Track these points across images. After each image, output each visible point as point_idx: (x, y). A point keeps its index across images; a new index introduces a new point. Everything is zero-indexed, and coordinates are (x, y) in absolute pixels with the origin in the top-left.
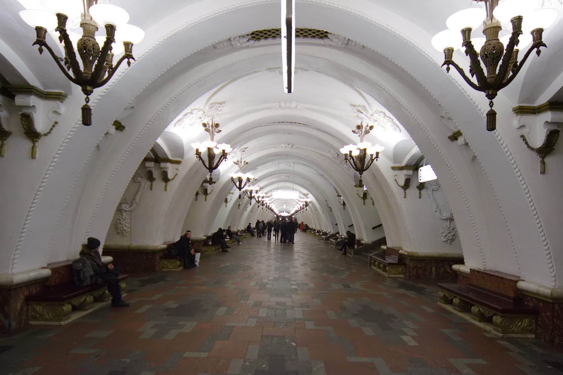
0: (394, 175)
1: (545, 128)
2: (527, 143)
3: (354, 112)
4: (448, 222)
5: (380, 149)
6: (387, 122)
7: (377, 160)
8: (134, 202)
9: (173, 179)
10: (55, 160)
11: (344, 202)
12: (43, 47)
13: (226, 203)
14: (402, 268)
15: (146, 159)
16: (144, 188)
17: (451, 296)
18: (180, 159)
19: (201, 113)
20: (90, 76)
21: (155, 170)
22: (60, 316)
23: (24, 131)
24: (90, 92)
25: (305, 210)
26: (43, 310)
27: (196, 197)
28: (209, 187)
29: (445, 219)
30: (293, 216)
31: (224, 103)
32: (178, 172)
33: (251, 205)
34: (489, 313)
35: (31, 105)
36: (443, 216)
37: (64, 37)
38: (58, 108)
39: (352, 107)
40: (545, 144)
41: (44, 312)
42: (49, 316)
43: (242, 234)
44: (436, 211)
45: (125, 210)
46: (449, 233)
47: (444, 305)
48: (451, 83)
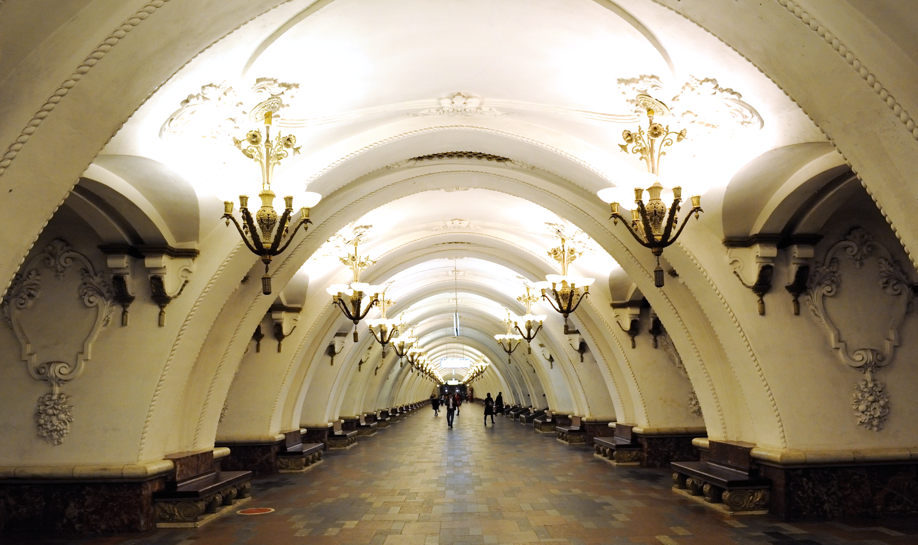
0: (731, 262)
5: (590, 282)
8: (80, 356)
9: (288, 335)
12: (230, 220)
13: (162, 307)
14: (636, 452)
16: (108, 321)
17: (700, 483)
18: (299, 306)
27: (359, 366)
28: (286, 319)
29: (859, 367)
30: (468, 385)
32: (383, 362)
33: (401, 363)
36: (854, 360)
43: (368, 424)
44: (837, 347)
45: (60, 380)
47: (680, 490)
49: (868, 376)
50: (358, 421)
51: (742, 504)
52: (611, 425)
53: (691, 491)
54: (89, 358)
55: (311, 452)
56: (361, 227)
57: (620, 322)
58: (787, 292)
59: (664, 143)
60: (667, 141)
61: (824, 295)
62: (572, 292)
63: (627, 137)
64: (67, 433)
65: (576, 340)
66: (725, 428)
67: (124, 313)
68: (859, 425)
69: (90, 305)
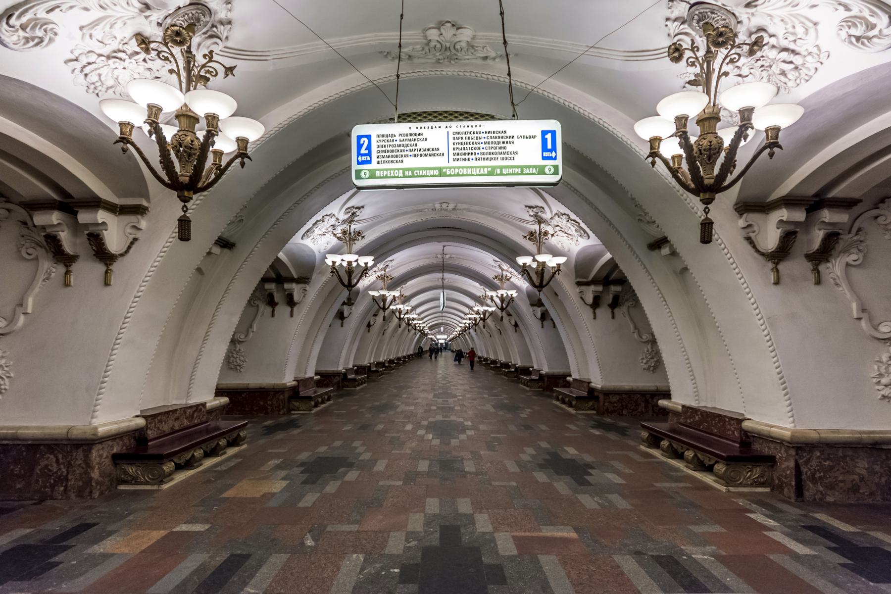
1: (778, 228)
2: (584, 301)
3: (530, 215)
4: (650, 344)
5: (561, 260)
6: (570, 226)
7: (559, 274)
8: (19, 310)
10: (142, 288)
11: (516, 323)
15: (265, 280)
19: (334, 219)
20: (187, 178)
21: (277, 291)
22: (161, 479)
23: (94, 253)
24: (188, 199)
25: (482, 327)
26: (136, 471)
31: (363, 207)
32: (139, 235)
34: (709, 461)
35: (100, 221)
37: (156, 129)
38: (138, 222)
39: (527, 208)
40: (780, 248)
41: (138, 474)
42: (144, 478)
45: (240, 341)
46: (652, 358)
48: (657, 176)
49: (649, 347)
50: (393, 361)
51: (738, 480)
52: (531, 369)
53: (646, 444)
54: (255, 330)
55: (360, 379)
56: (353, 207)
57: (753, 238)
58: (608, 308)
59: (728, 60)
60: (733, 57)
61: (848, 265)
62: (543, 269)
63: (674, 52)
64: (5, 389)
65: (539, 311)
66: (695, 383)
67: (273, 312)
68: (880, 399)
69: (31, 257)
